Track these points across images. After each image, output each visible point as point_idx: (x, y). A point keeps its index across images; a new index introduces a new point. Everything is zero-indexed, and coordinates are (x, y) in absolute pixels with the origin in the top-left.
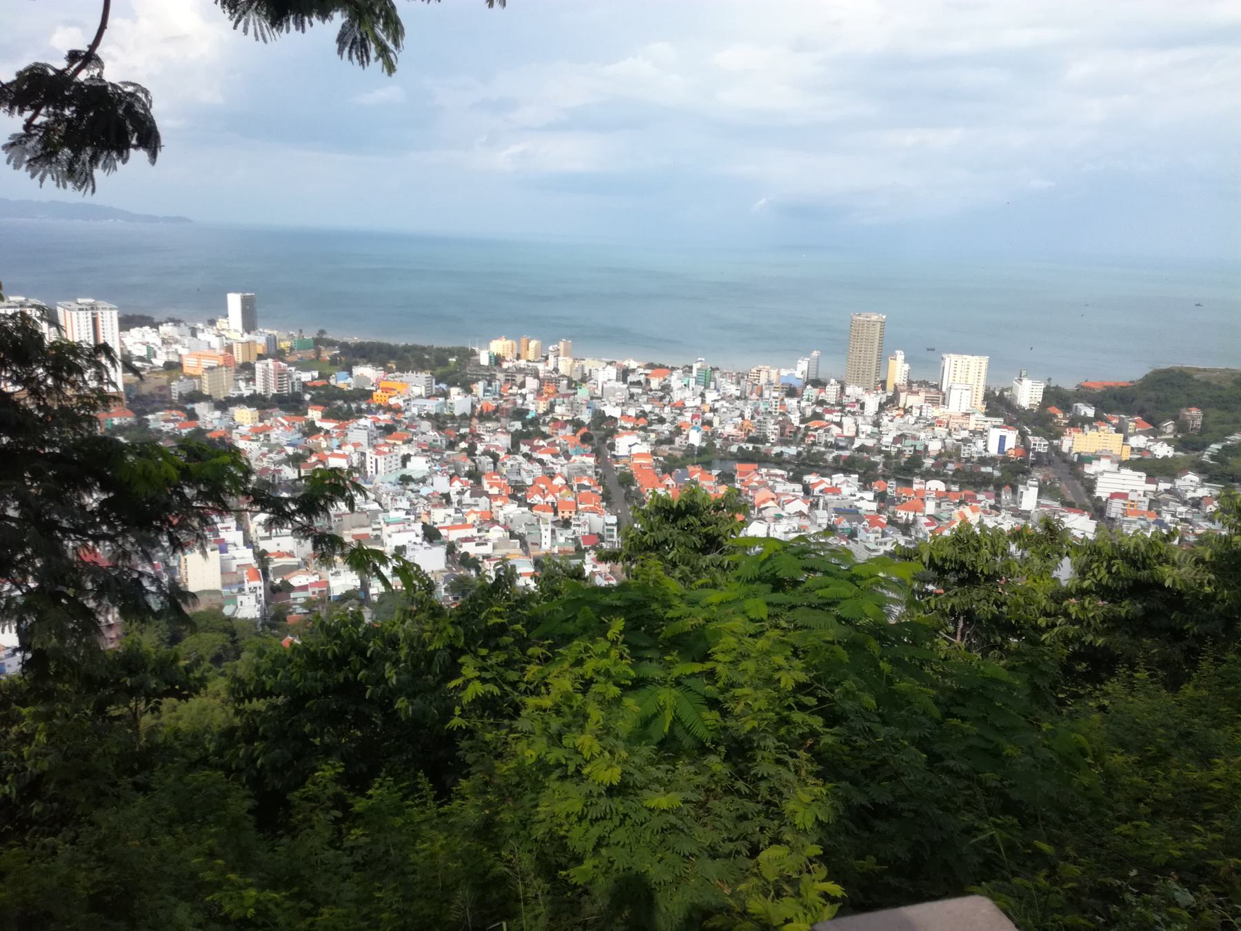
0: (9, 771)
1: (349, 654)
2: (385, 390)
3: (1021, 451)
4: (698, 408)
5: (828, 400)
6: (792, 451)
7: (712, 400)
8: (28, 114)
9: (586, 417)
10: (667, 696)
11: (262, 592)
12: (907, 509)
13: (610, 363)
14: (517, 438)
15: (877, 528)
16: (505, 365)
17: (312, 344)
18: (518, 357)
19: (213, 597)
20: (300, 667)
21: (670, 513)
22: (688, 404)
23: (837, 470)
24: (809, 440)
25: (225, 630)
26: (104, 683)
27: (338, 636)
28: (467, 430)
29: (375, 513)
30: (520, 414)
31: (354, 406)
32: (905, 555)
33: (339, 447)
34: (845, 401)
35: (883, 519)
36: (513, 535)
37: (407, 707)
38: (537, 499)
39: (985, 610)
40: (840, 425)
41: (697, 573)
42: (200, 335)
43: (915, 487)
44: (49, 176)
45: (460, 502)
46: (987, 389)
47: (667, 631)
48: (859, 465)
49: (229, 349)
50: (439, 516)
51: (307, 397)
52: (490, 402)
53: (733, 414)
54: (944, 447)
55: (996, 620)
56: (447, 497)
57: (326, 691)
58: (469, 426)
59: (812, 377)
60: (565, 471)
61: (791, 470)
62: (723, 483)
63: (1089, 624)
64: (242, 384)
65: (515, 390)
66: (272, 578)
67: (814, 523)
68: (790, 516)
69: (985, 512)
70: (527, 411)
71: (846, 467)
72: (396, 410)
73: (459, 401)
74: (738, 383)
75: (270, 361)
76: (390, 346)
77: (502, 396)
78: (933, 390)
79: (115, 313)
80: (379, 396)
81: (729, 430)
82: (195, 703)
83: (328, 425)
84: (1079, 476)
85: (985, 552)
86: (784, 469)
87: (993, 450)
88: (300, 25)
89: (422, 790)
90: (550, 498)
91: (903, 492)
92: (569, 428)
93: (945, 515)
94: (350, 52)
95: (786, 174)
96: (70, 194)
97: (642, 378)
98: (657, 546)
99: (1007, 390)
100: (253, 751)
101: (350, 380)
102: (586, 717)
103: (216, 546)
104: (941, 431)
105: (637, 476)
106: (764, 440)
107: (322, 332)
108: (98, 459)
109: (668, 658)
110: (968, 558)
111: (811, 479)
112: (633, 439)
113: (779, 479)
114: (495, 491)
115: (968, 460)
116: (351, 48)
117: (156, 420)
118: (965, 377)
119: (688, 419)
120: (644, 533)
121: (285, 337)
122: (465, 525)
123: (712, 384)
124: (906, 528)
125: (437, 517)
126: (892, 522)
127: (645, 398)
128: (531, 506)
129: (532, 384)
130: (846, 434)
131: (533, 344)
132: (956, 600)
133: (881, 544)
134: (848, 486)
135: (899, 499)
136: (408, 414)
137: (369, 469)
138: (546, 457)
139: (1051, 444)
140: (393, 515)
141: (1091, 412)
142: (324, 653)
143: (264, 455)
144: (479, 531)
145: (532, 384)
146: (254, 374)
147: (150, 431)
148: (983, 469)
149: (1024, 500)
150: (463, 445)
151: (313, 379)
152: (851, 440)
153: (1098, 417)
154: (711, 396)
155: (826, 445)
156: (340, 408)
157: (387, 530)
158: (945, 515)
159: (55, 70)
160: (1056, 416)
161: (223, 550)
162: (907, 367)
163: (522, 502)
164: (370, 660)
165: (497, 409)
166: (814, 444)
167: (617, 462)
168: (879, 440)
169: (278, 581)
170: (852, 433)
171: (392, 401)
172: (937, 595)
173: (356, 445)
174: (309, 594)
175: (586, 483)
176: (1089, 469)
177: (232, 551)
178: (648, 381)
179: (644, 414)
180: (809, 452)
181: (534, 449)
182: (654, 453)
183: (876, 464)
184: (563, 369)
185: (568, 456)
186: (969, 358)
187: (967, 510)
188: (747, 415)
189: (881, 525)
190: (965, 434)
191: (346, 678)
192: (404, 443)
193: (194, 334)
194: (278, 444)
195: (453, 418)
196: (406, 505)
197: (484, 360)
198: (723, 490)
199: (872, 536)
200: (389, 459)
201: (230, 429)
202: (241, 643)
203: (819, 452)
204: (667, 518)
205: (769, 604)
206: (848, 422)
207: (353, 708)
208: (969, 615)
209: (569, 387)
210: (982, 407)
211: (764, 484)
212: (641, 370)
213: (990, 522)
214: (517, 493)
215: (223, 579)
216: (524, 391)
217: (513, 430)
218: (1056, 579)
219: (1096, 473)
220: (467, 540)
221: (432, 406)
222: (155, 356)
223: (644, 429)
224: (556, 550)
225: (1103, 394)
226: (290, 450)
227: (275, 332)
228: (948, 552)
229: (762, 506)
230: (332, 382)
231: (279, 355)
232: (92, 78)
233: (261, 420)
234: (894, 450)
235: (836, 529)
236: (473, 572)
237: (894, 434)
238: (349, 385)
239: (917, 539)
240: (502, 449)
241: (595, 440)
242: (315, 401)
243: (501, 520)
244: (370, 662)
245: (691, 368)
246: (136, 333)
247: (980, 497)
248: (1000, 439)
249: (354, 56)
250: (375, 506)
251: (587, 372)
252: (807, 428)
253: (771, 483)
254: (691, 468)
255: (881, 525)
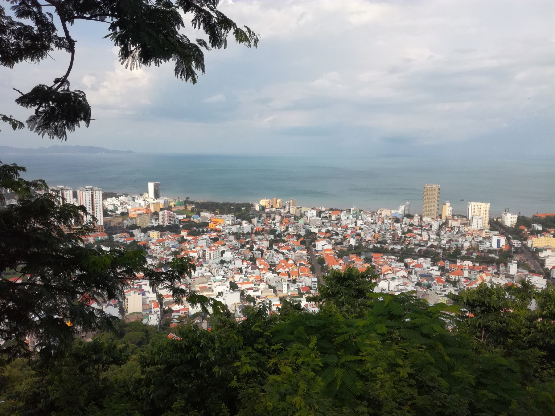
0: (42, 398)
1: (192, 346)
2: (214, 222)
3: (508, 247)
4: (354, 228)
5: (415, 224)
6: (399, 247)
7: (361, 222)
8: (37, 107)
9: (302, 233)
10: (338, 372)
11: (160, 313)
12: (455, 274)
13: (313, 209)
14: (272, 243)
15: (441, 283)
16: (266, 210)
17: (183, 203)
18: (272, 207)
19: (139, 315)
20: (170, 351)
21: (339, 279)
22: (349, 226)
23: (420, 256)
24: (406, 243)
25: (143, 331)
26: (84, 358)
27: (187, 337)
28: (250, 239)
29: (209, 277)
30: (273, 232)
31: (201, 229)
32: (455, 299)
33: (194, 248)
34: (423, 224)
35: (444, 279)
36: (270, 287)
37: (219, 372)
38: (281, 270)
39: (495, 325)
40: (421, 235)
41: (354, 308)
42: (136, 201)
43: (458, 264)
44: (46, 134)
45: (246, 272)
46: (490, 218)
47: (338, 340)
48: (431, 254)
49: (149, 206)
50: (237, 278)
51: (181, 226)
52: (260, 227)
53: (370, 231)
54: (471, 245)
55: (500, 330)
56: (240, 269)
57: (182, 363)
58: (251, 237)
59: (407, 213)
60: (293, 257)
61: (399, 256)
62: (367, 262)
63: (547, 332)
64: (153, 221)
65: (271, 221)
66: (164, 307)
67: (410, 281)
68: (399, 278)
69: (492, 275)
70: (276, 231)
71: (425, 255)
72: (219, 231)
73: (246, 227)
74: (372, 217)
75: (165, 211)
76: (216, 203)
77: (265, 224)
78: (464, 219)
79: (101, 192)
80: (211, 225)
81: (369, 238)
82: (129, 363)
83: (189, 238)
84: (537, 258)
85: (494, 297)
86: (395, 256)
87: (495, 246)
88: (157, 63)
89: (224, 412)
90: (287, 270)
91: (453, 266)
92: (295, 238)
93: (473, 277)
94: (181, 75)
95: (390, 124)
96: (56, 141)
97: (328, 215)
98: (334, 295)
99: (499, 218)
100: (149, 390)
101: (199, 218)
102: (298, 386)
103: (141, 292)
104: (469, 238)
105: (326, 259)
106: (385, 242)
107: (188, 198)
108: (82, 257)
109: (339, 353)
110: (486, 300)
111: (408, 260)
112: (324, 242)
113: (393, 261)
114: (262, 267)
115: (483, 251)
116: (182, 73)
117: (117, 237)
118: (479, 212)
119: (349, 233)
120: (328, 289)
121: (172, 200)
122: (249, 282)
123: (360, 217)
124: (454, 284)
125: (233, 282)
126: (448, 281)
127: (329, 224)
128: (278, 274)
129: (278, 218)
130: (424, 239)
131: (278, 201)
132: (481, 321)
133: (443, 291)
134: (426, 263)
135: (451, 270)
136: (224, 233)
137: (207, 257)
138: (285, 251)
139: (522, 243)
140: (217, 278)
141: (540, 228)
142: (181, 345)
143: (162, 252)
144: (255, 285)
145: (278, 218)
146: (159, 217)
147: (114, 242)
148: (490, 255)
149: (511, 270)
150: (248, 246)
151: (184, 218)
152: (426, 242)
153: (544, 230)
154: (359, 223)
155: (415, 245)
156: (195, 231)
157: (214, 285)
158: (473, 277)
159: (48, 87)
160: (524, 230)
161: (143, 294)
162: (451, 208)
163: (274, 272)
164: (202, 348)
165: (263, 230)
166: (409, 244)
167: (317, 253)
168: (440, 242)
169: (167, 308)
170: (427, 239)
171: (217, 227)
172: (471, 318)
173: (201, 247)
174: (180, 314)
175: (303, 263)
176: (542, 255)
177: (147, 295)
178: (330, 216)
179: (329, 231)
180: (406, 248)
181: (279, 247)
182: (334, 249)
183: (439, 253)
184: (292, 211)
185: (294, 251)
186: (481, 204)
187: (483, 275)
188: (377, 231)
189: (442, 282)
190: (481, 239)
191: (191, 357)
192: (222, 245)
193: (134, 200)
194: (168, 247)
195: (243, 234)
196: (223, 273)
197: (257, 208)
198: (367, 265)
199: (439, 287)
200: (215, 253)
201: (148, 241)
202: (150, 336)
203: (411, 248)
204: (339, 282)
205: (387, 327)
206: (425, 234)
207: (193, 371)
208: (487, 328)
209: (295, 219)
210: (487, 226)
211: (386, 263)
212: (327, 212)
213: (496, 281)
214: (272, 267)
215: (143, 307)
216: (275, 222)
217: (270, 239)
218: (529, 310)
219: (545, 257)
220: (249, 289)
221: (234, 229)
222: (117, 210)
223: (329, 238)
224: (290, 294)
225: (546, 219)
226: (173, 249)
227: (168, 199)
228: (476, 297)
229: (386, 273)
230: (192, 219)
231: (169, 208)
232: (64, 90)
233: (161, 236)
234: (447, 247)
235: (421, 284)
236: (252, 304)
237: (446, 239)
238: (199, 221)
239: (460, 289)
240: (265, 248)
241: (307, 243)
242: (184, 228)
243: (265, 279)
244: (201, 350)
245: (350, 210)
246: (109, 200)
247: (489, 268)
248: (497, 241)
249: (183, 77)
250: (209, 274)
251: (303, 212)
252: (405, 237)
253: (389, 262)
254: (351, 256)
255: (442, 282)
